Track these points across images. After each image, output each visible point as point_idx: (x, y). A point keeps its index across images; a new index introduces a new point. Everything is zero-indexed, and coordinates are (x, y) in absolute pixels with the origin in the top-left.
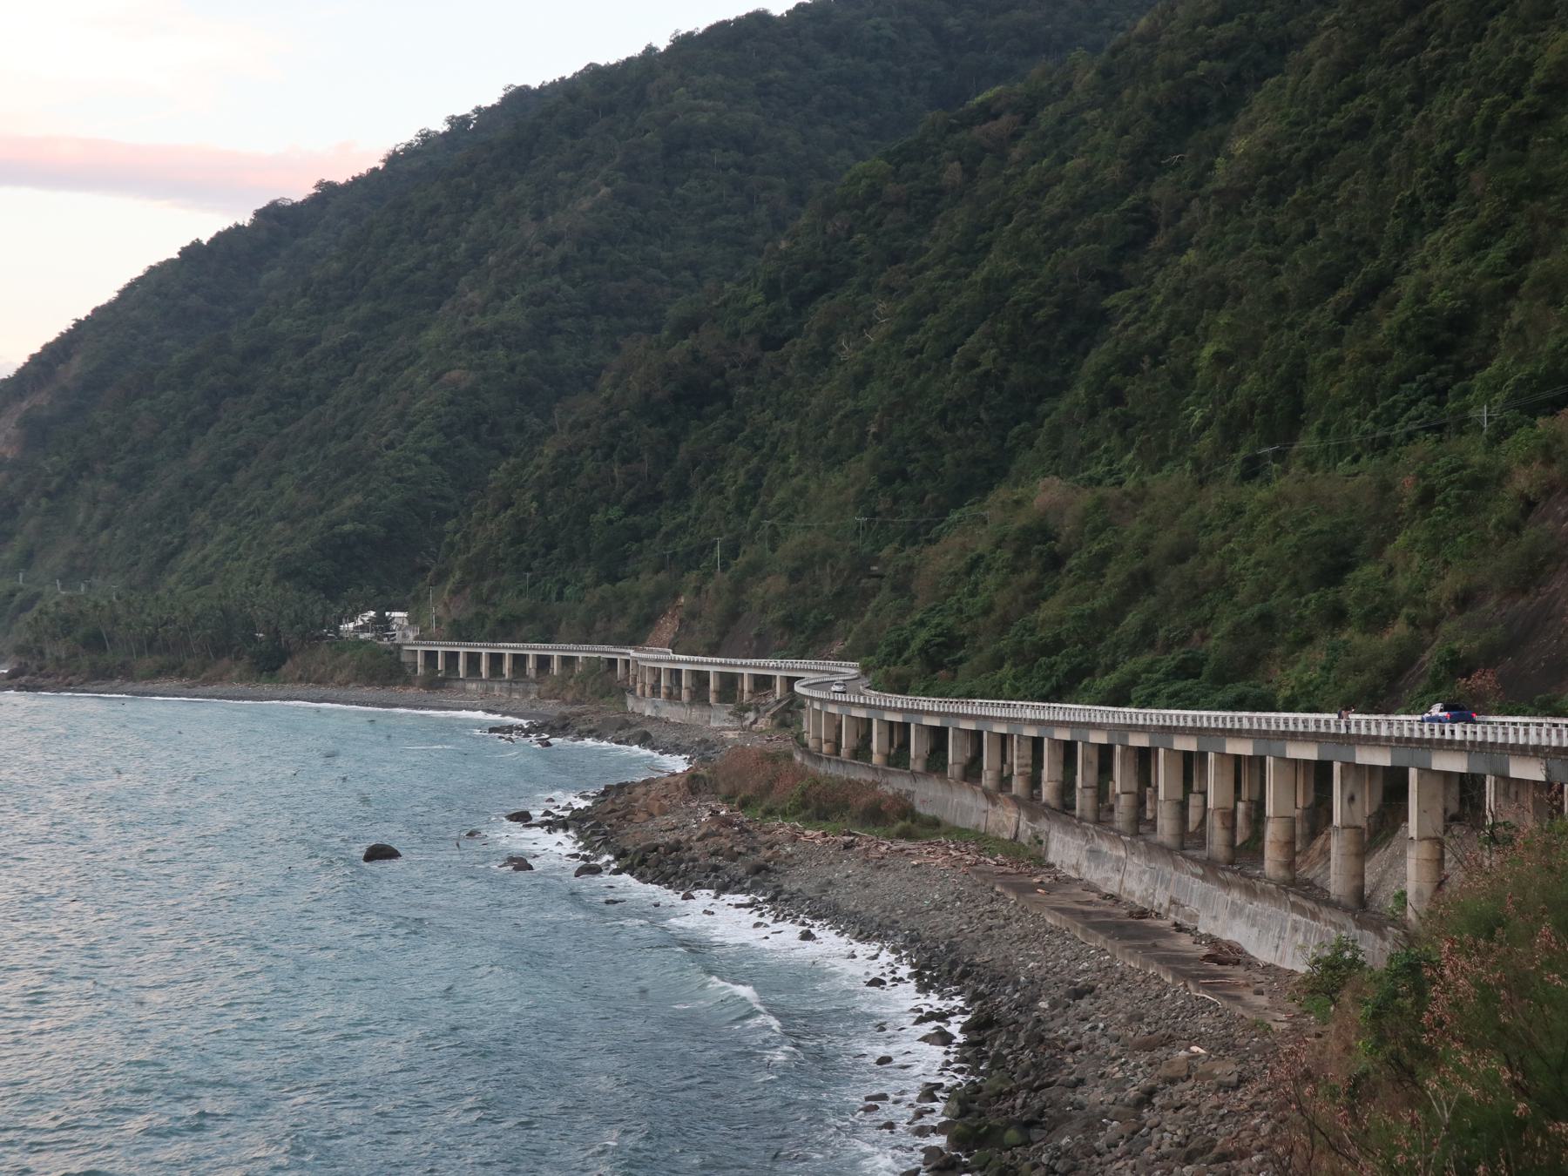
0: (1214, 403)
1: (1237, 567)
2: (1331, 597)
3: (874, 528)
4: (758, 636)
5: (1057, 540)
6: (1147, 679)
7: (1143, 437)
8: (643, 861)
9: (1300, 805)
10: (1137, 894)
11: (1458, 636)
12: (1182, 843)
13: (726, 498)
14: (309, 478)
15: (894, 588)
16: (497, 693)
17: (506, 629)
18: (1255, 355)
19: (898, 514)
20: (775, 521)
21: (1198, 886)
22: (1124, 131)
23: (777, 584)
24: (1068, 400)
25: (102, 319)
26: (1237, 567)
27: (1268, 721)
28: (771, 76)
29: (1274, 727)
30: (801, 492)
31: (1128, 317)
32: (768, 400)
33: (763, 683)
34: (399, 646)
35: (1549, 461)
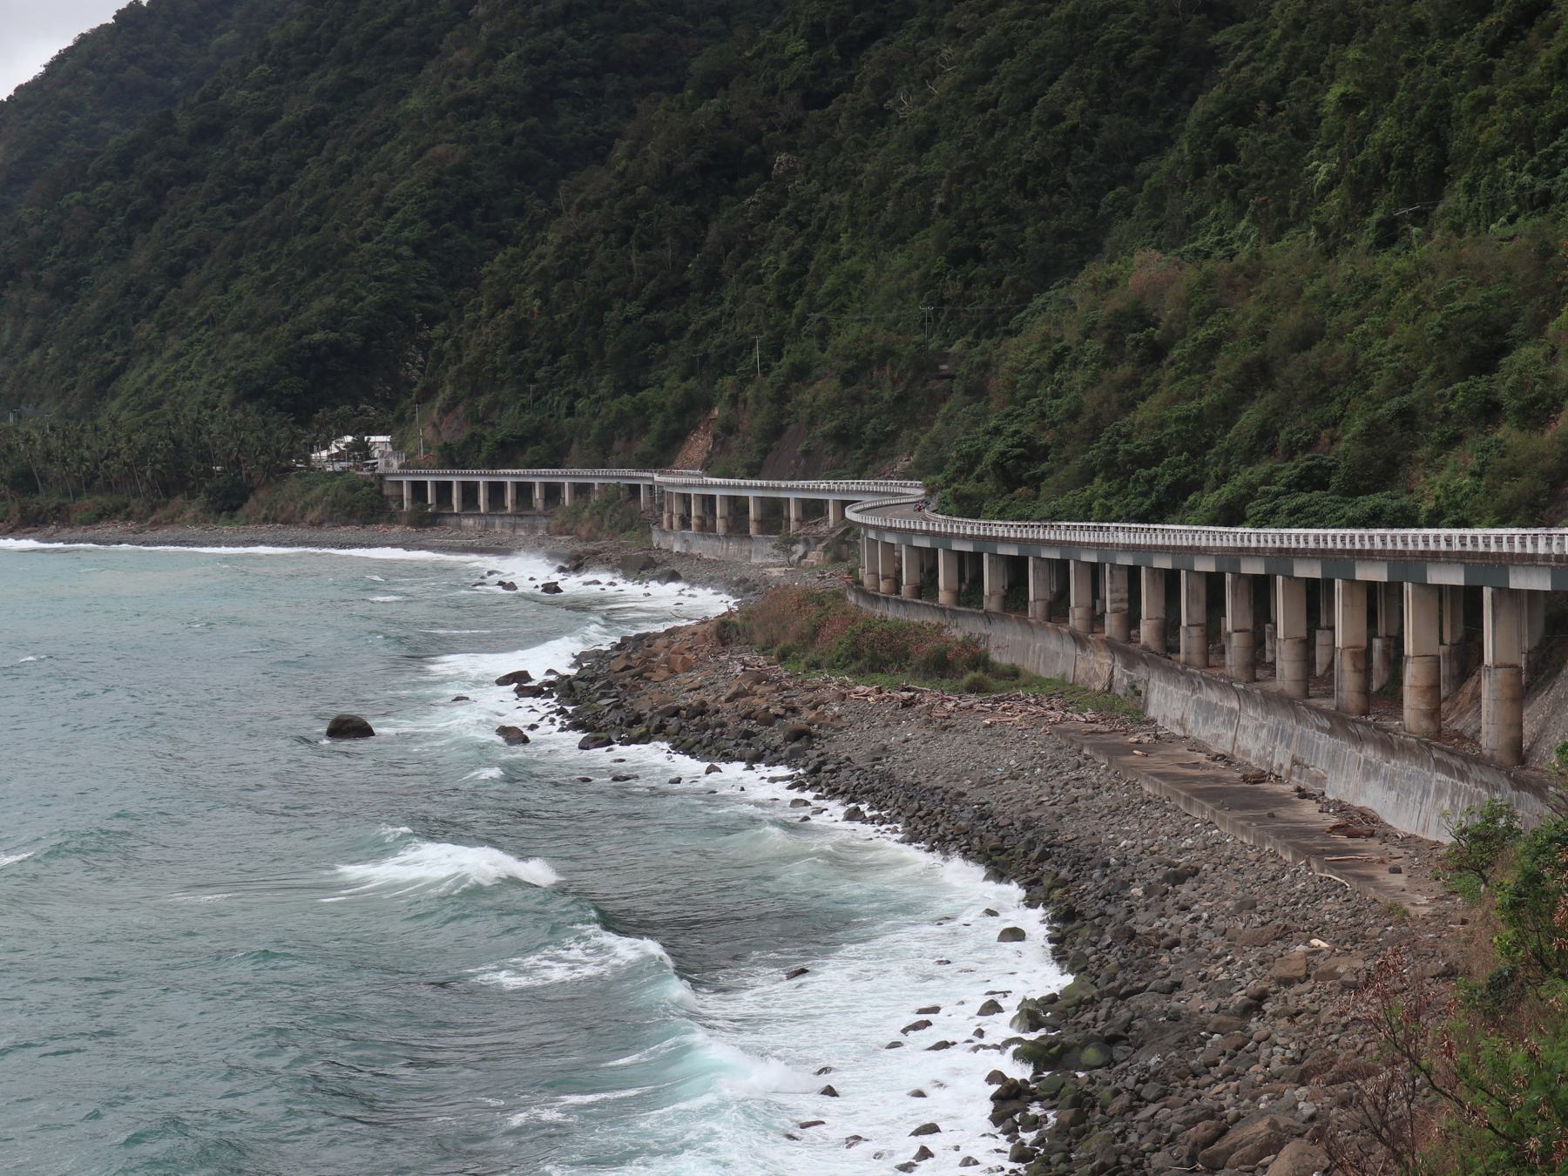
0: (1341, 155)
1: (1372, 352)
2: (1482, 386)
3: (943, 319)
4: (807, 453)
5: (1157, 327)
6: (1266, 493)
7: (1259, 200)
9: (1447, 639)
10: (1253, 754)
12: (1307, 691)
13: (766, 288)
16: (498, 529)
17: (506, 454)
18: (1391, 96)
19: (970, 300)
20: (823, 313)
21: (1324, 741)
24: (1171, 158)
26: (1372, 352)
27: (1404, 539)
29: (1411, 547)
31: (1242, 56)
32: (813, 168)
34: (381, 477)
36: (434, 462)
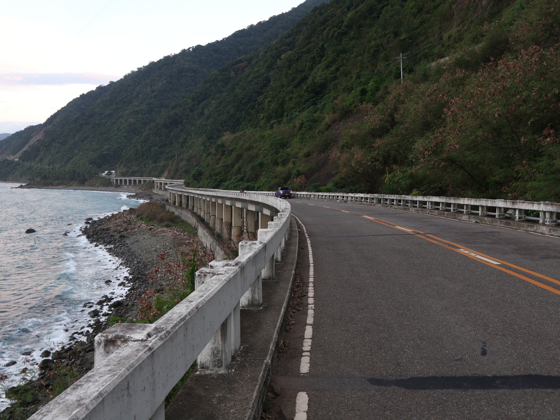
4: (180, 175)
17: (133, 174)
22: (266, 62)
25: (63, 110)
28: (202, 58)
35: (334, 112)
36: (120, 175)
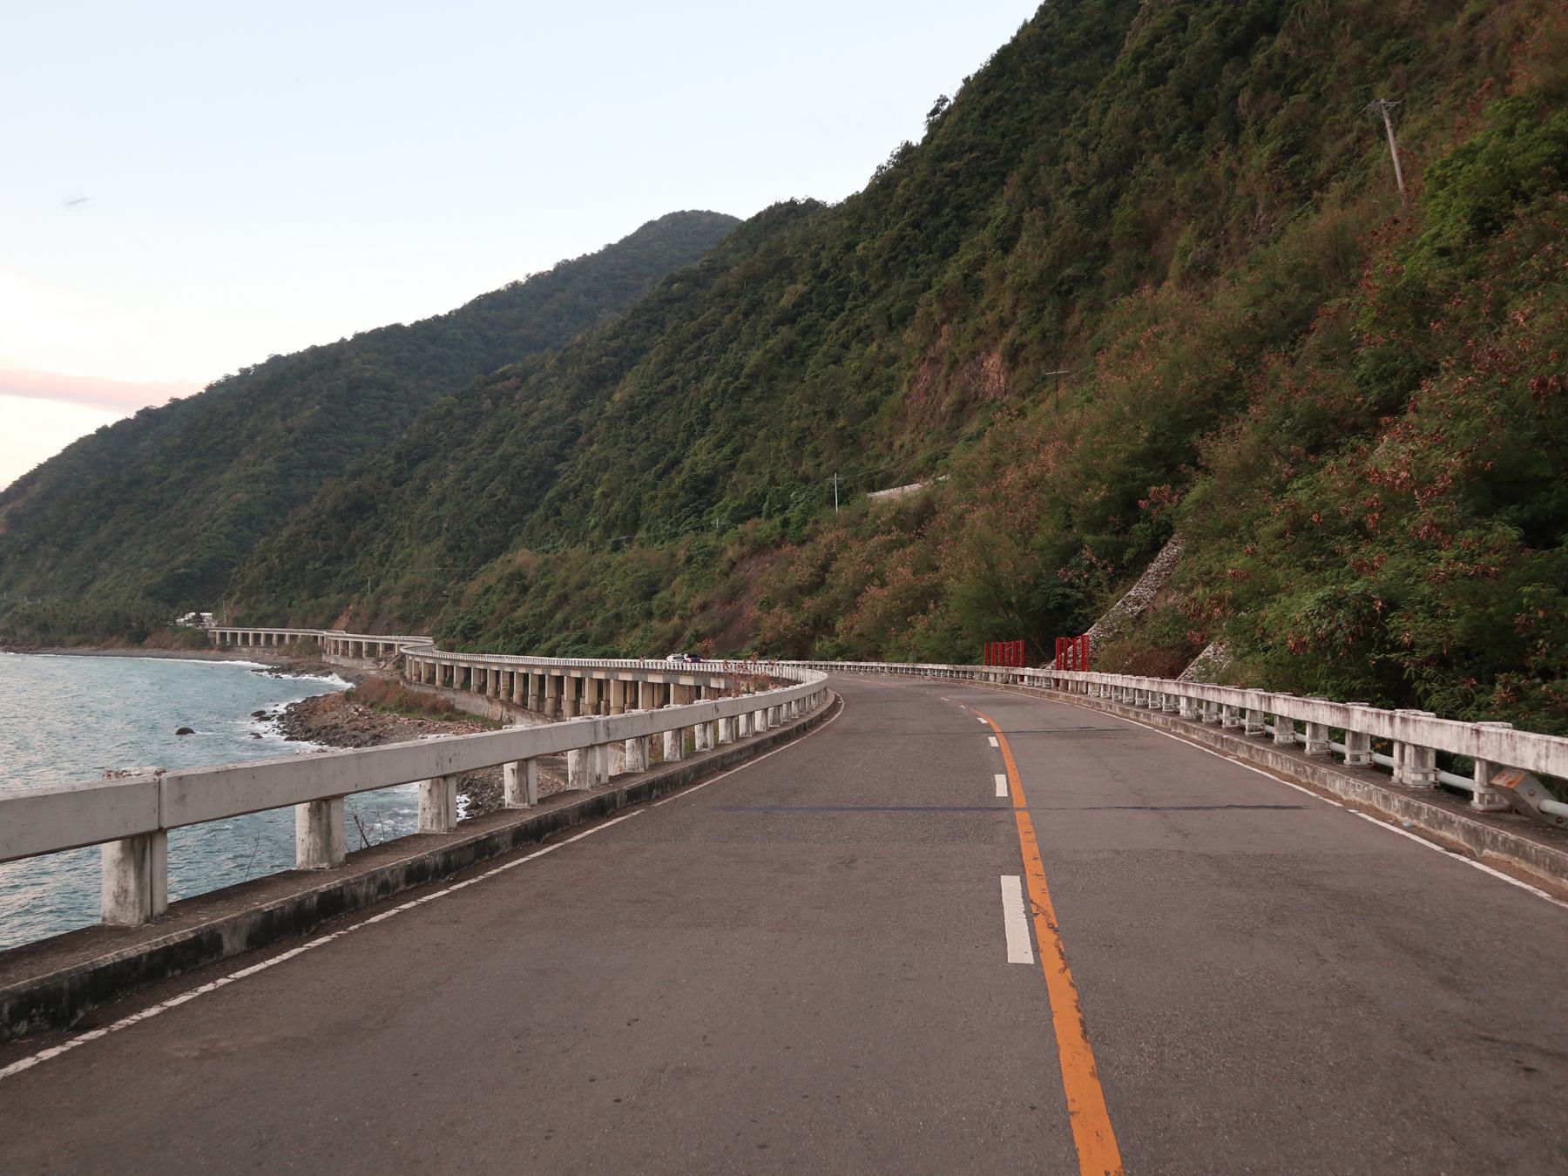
4: (387, 624)
8: (319, 734)
11: (700, 624)
14: (162, 546)
15: (454, 602)
17: (261, 622)
18: (620, 494)
22: (568, 387)
23: (396, 599)
25: (53, 463)
30: (410, 555)
33: (389, 647)
34: (207, 630)
35: (742, 544)
